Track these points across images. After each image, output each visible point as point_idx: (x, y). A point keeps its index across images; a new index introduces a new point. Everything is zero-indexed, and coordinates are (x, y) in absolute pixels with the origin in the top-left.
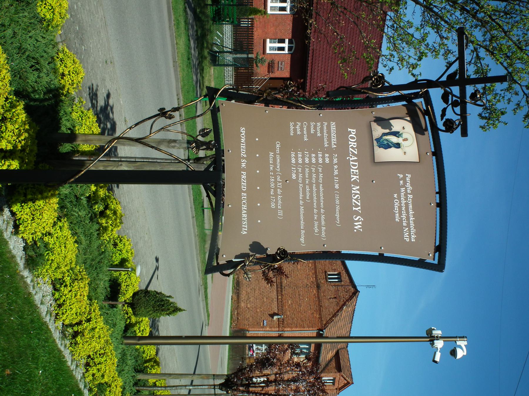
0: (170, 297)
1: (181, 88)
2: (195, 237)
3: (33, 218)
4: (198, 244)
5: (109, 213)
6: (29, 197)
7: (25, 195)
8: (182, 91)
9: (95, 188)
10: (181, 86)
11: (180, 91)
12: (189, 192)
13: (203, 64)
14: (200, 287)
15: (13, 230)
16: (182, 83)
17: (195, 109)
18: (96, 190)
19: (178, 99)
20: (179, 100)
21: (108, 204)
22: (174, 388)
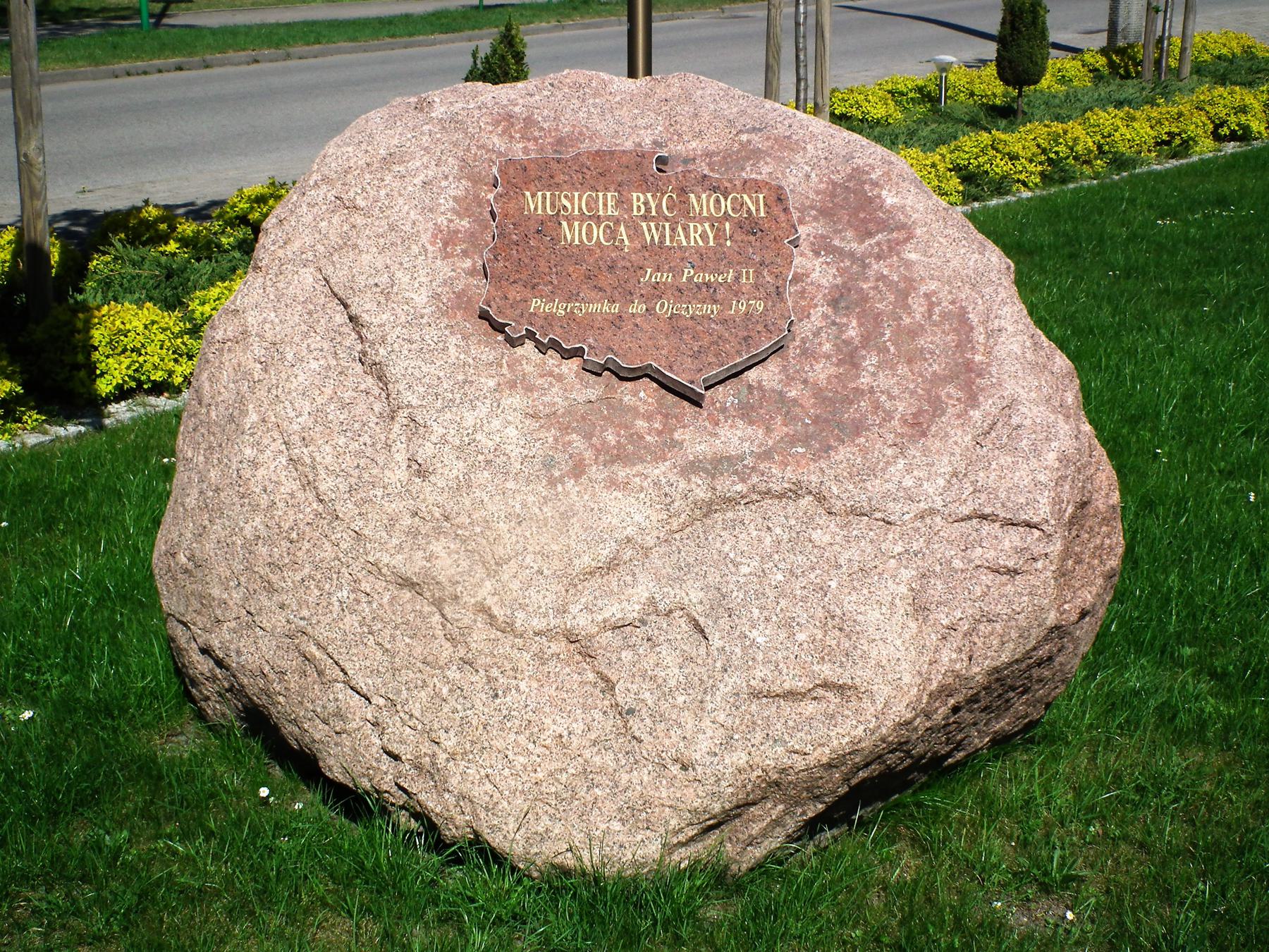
0: (474, 55)
1: (97, 65)
2: (563, 28)
3: (132, 351)
4: (587, 21)
5: (257, 214)
6: (80, 358)
7: (77, 367)
8: (104, 64)
9: (172, 242)
10: (90, 65)
11: (104, 67)
12: (420, 44)
13: (63, 9)
14: (726, 15)
15: (166, 394)
16: (80, 63)
17: (175, 30)
18: (177, 240)
19: (129, 74)
20: (133, 71)
21: (237, 217)
22: (802, 57)
